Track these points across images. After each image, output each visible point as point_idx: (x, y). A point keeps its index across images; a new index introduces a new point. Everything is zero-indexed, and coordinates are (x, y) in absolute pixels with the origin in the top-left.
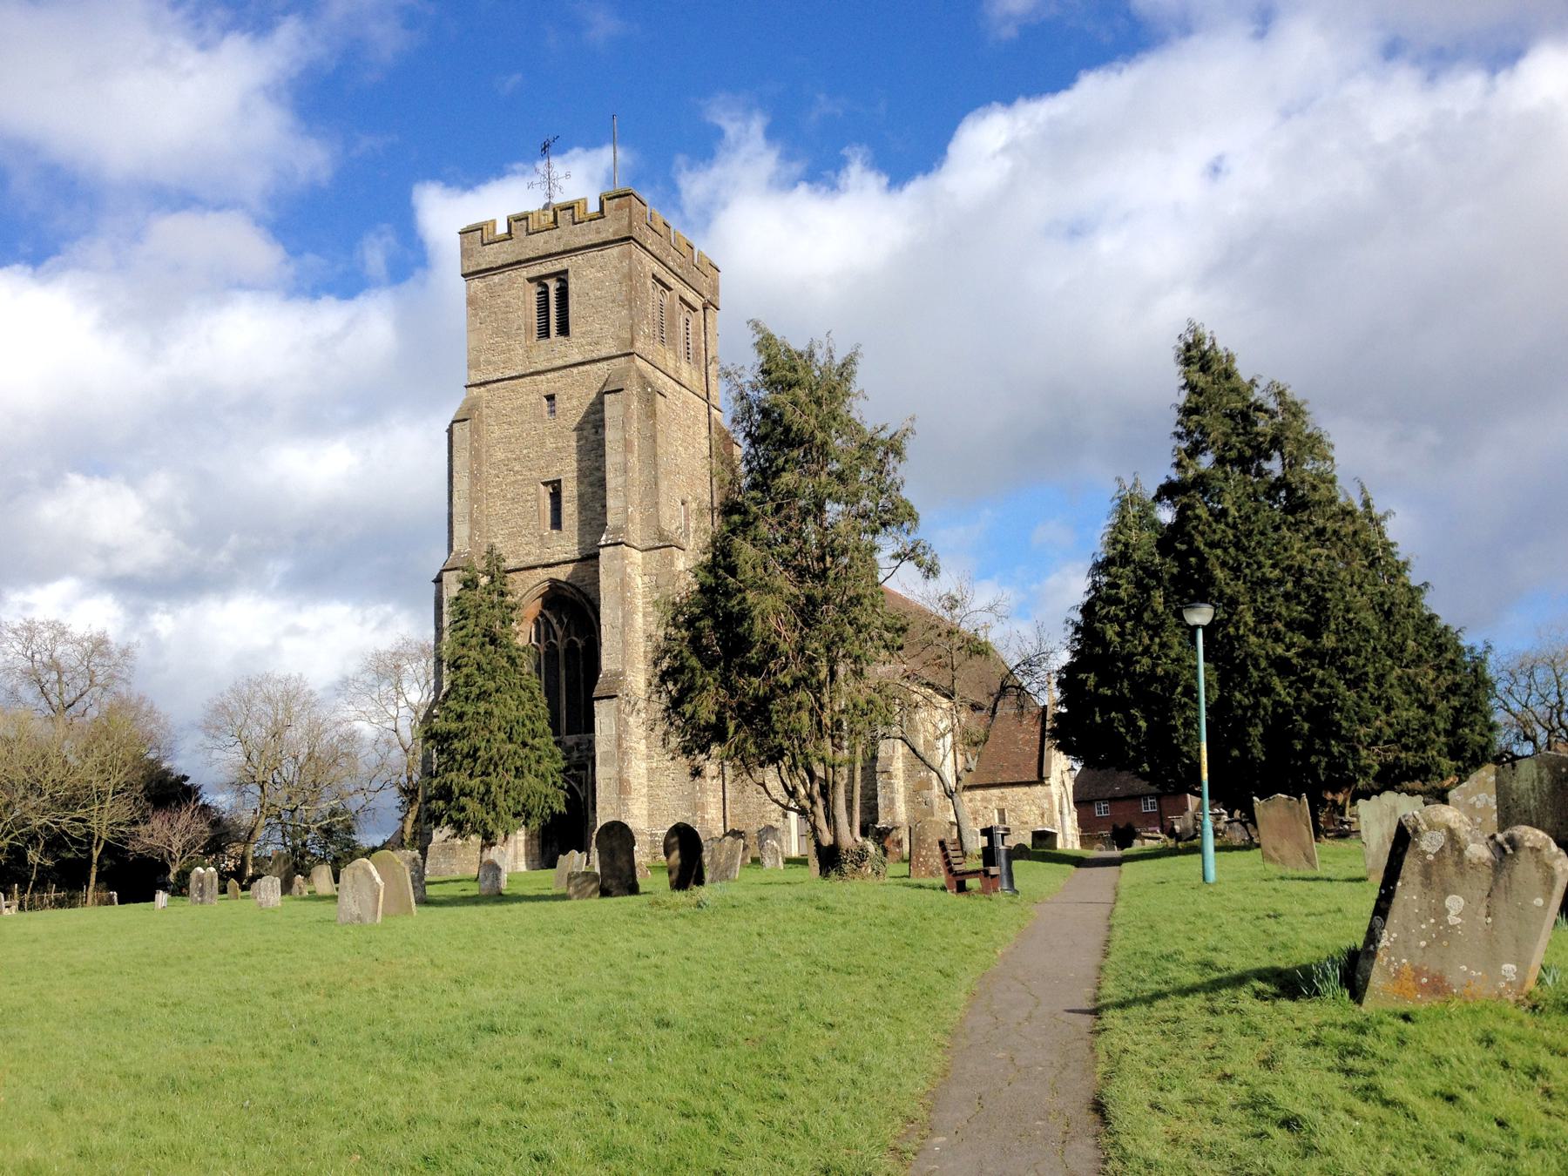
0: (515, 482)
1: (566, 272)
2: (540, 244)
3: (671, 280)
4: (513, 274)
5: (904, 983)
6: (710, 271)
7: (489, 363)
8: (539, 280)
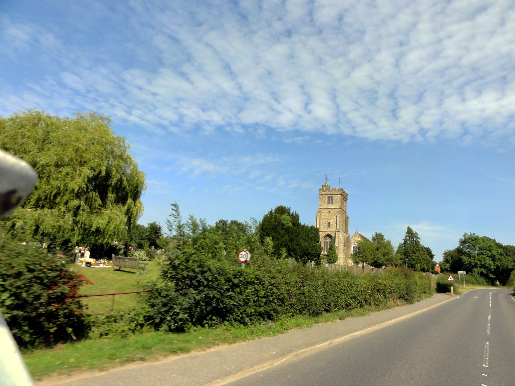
2: (330, 193)
8: (329, 197)
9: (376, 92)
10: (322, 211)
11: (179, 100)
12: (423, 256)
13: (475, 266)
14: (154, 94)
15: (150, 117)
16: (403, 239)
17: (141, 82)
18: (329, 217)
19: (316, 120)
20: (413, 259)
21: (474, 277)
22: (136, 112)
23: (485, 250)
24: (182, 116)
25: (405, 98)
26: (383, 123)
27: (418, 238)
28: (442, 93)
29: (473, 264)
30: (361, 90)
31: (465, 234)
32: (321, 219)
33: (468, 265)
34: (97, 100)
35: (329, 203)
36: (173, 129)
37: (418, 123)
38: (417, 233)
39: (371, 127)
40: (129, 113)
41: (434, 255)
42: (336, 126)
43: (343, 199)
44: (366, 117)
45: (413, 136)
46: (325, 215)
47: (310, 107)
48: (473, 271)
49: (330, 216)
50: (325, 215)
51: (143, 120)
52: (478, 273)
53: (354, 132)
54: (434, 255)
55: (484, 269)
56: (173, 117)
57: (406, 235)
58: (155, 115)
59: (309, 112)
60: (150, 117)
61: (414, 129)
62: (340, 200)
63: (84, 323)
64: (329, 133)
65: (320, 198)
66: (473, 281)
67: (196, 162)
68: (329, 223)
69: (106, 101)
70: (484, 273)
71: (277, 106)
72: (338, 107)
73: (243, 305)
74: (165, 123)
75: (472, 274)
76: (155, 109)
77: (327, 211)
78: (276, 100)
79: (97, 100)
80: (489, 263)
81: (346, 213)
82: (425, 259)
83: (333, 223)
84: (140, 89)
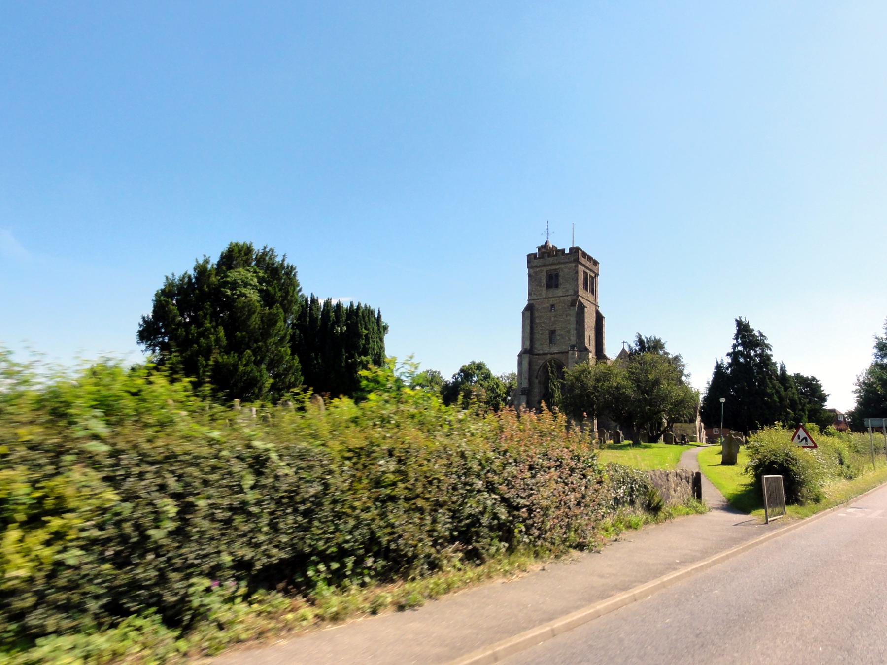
3: (588, 271)
4: (542, 268)
18: (553, 319)
27: (768, 347)
41: (828, 395)
49: (555, 317)
54: (828, 395)
63: (311, 584)
73: (441, 506)
81: (596, 306)
83: (562, 333)
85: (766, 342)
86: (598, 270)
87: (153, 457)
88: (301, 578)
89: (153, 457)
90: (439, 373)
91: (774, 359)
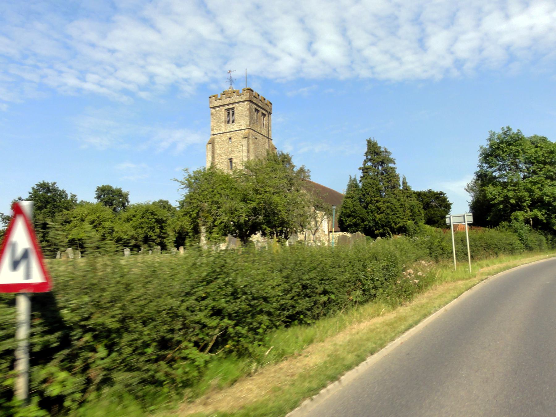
0: (310, 271)
1: (234, 108)
2: (228, 101)
3: (259, 109)
5: (142, 228)
6: (269, 104)
7: (216, 129)
9: (396, 18)
10: (217, 139)
11: (145, 55)
12: (402, 199)
13: (518, 206)
14: (112, 51)
15: (111, 82)
16: (360, 169)
17: (92, 36)
18: (230, 149)
19: (324, 62)
20: (379, 208)
21: (516, 231)
22: (91, 77)
23: (541, 163)
24: (152, 76)
25: (434, 22)
26: (409, 57)
27: (392, 161)
28: (479, 10)
29: (513, 201)
30: (377, 17)
31: (492, 135)
32: (216, 156)
33: (501, 206)
34: (38, 68)
35: (229, 122)
36: (143, 95)
37: (452, 53)
38: (388, 151)
39: (394, 64)
40: (83, 79)
41: (452, 204)
42: (350, 67)
43: (256, 110)
44: (386, 52)
45: (447, 71)
46: (222, 146)
47: (315, 46)
48: (512, 218)
49: (231, 148)
50: (222, 146)
51: (102, 86)
52: (527, 221)
53: (373, 73)
54: (452, 204)
55: (541, 211)
56: (141, 78)
57: (365, 158)
58: (117, 78)
59: (314, 54)
60: (111, 82)
61: (448, 62)
62: (248, 112)
64: (342, 77)
65: (212, 114)
66: (511, 244)
67: (178, 135)
68: (231, 160)
69: (51, 67)
70: (542, 220)
71: (272, 50)
72: (350, 43)
74: (131, 87)
75: (510, 226)
76: (116, 71)
77: (225, 137)
78: (270, 42)
79: (38, 68)
80: (552, 194)
82: (407, 205)
84: (93, 45)
85: (390, 157)
86: (271, 109)
87: (97, 252)
88: (65, 313)
89: (97, 252)
90: (98, 187)
91: (397, 172)
